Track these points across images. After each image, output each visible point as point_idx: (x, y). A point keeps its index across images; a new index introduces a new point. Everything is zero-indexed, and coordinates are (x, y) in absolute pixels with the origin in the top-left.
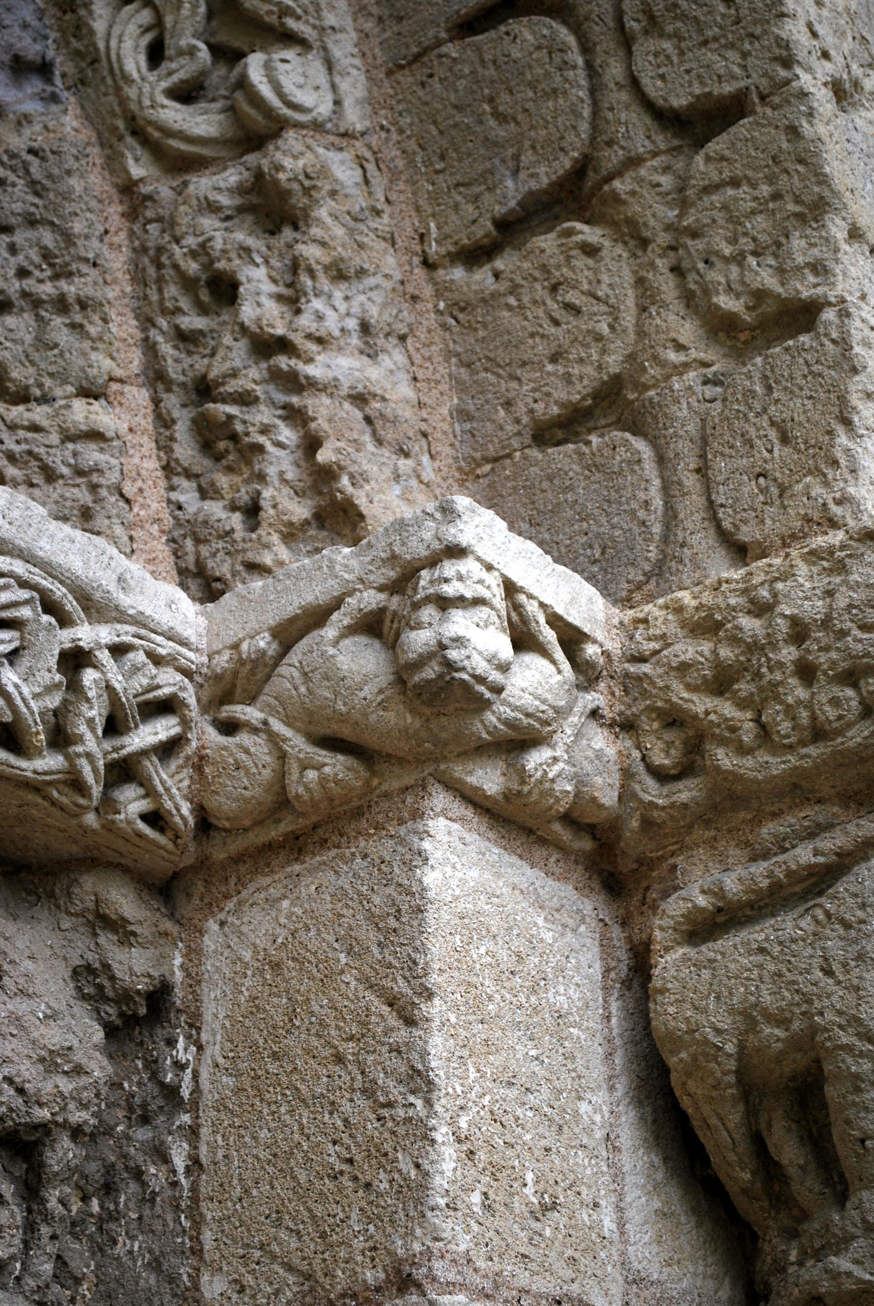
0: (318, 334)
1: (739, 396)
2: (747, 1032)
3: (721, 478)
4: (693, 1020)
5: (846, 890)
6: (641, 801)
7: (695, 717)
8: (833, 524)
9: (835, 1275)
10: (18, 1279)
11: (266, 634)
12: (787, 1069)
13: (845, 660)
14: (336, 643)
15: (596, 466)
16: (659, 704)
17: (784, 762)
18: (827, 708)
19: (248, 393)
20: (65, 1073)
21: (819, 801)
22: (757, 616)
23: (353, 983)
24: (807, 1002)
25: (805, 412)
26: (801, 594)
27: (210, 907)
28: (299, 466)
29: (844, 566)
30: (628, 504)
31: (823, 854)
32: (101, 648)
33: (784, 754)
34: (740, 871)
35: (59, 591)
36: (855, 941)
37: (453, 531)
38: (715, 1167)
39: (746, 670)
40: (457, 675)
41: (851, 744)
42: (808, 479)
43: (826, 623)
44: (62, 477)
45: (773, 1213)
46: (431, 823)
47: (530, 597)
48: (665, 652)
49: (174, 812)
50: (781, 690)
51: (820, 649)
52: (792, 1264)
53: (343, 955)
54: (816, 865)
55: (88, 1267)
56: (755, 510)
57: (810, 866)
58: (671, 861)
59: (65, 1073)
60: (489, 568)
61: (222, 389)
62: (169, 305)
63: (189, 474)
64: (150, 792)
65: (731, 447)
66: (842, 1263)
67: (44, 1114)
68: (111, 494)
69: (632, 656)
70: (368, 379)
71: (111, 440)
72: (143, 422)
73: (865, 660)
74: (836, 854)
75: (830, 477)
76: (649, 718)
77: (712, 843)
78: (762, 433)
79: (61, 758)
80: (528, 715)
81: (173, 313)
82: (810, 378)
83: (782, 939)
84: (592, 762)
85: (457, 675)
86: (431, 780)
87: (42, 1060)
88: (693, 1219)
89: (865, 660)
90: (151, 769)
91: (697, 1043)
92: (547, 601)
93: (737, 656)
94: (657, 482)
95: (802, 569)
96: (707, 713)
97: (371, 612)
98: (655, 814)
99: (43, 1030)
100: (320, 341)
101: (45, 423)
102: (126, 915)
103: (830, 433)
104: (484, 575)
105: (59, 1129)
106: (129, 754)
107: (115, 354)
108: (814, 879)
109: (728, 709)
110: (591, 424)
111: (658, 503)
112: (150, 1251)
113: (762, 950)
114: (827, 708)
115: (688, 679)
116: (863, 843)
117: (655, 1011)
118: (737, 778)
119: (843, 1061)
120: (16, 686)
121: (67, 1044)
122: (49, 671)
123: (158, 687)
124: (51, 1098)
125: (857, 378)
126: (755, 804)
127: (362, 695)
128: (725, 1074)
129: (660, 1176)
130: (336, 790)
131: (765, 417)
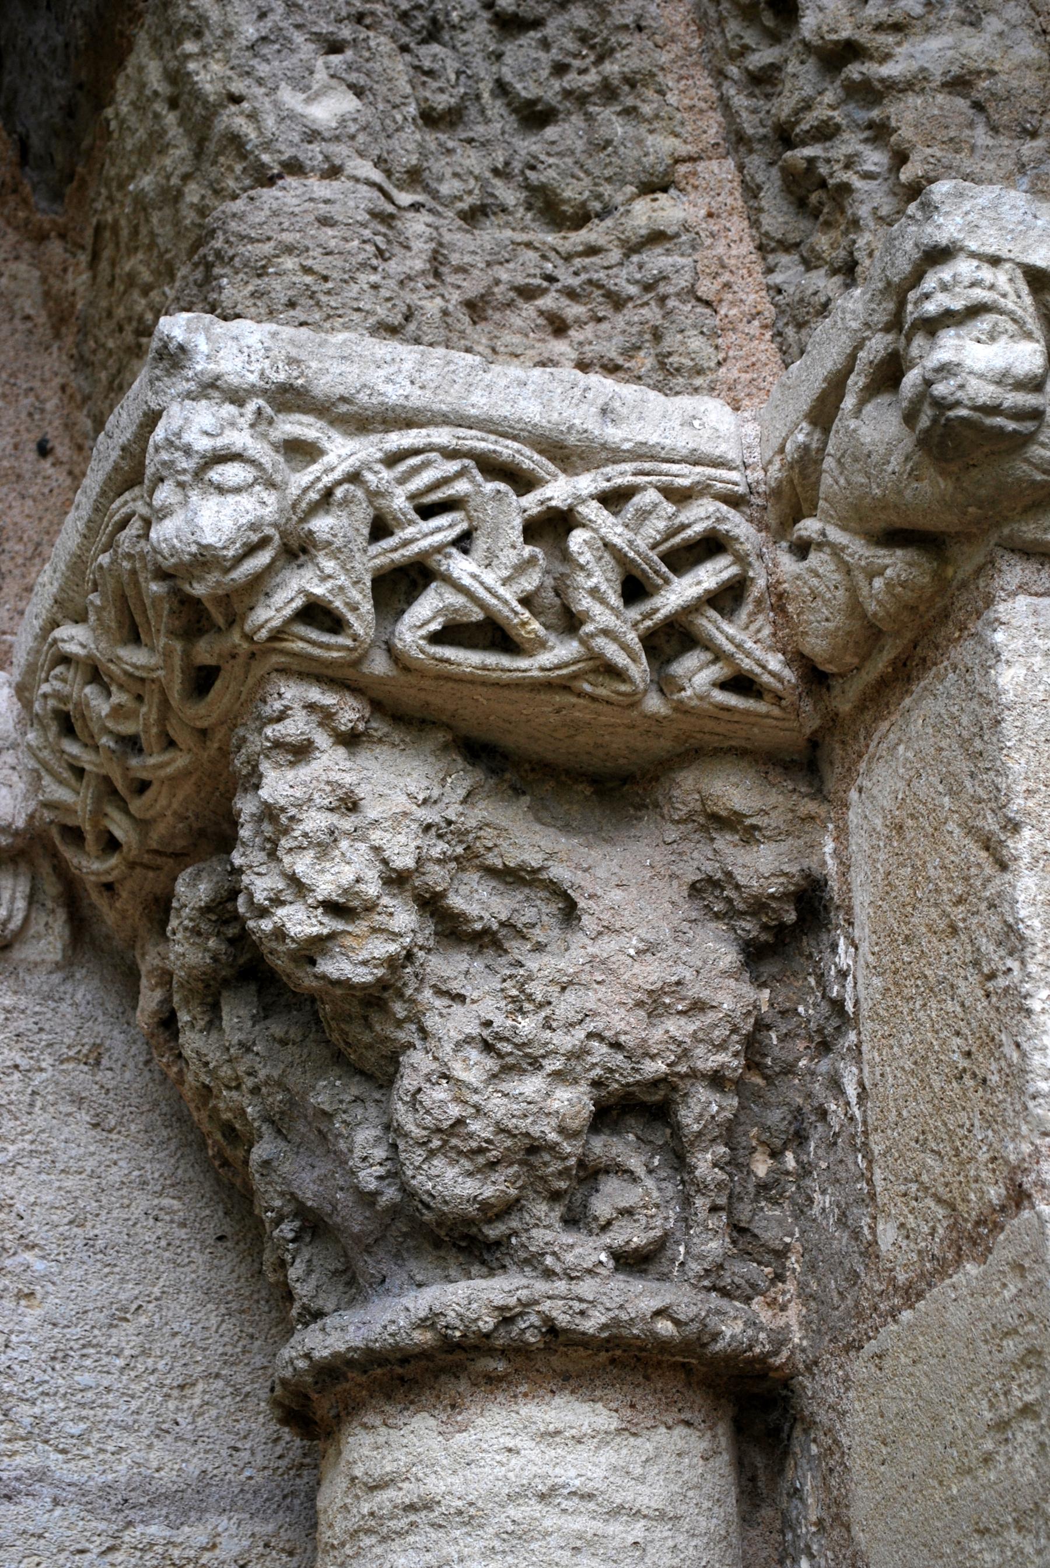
0: (891, 21)
10: (682, 1264)
11: (804, 424)
14: (857, 412)
19: (825, 123)
20: (679, 1013)
23: (957, 831)
27: (850, 774)
28: (895, 194)
32: (584, 501)
35: (507, 449)
40: (951, 414)
44: (630, 298)
46: (1001, 607)
49: (758, 670)
53: (946, 799)
55: (792, 1235)
59: (679, 1013)
60: (995, 261)
61: (797, 130)
62: (734, 46)
63: (786, 246)
64: (718, 656)
67: (660, 1067)
68: (684, 302)
70: (965, 56)
71: (677, 235)
72: (730, 201)
79: (575, 644)
81: (742, 55)
85: (951, 414)
86: (1000, 552)
87: (640, 1004)
90: (710, 627)
97: (883, 362)
99: (637, 968)
100: (897, 28)
101: (602, 241)
102: (737, 808)
104: (987, 274)
105: (688, 1082)
106: (667, 617)
107: (678, 129)
112: (838, 1206)
120: (474, 576)
121: (675, 979)
122: (514, 547)
123: (684, 527)
124: (662, 1047)
127: (890, 469)
130: (909, 596)
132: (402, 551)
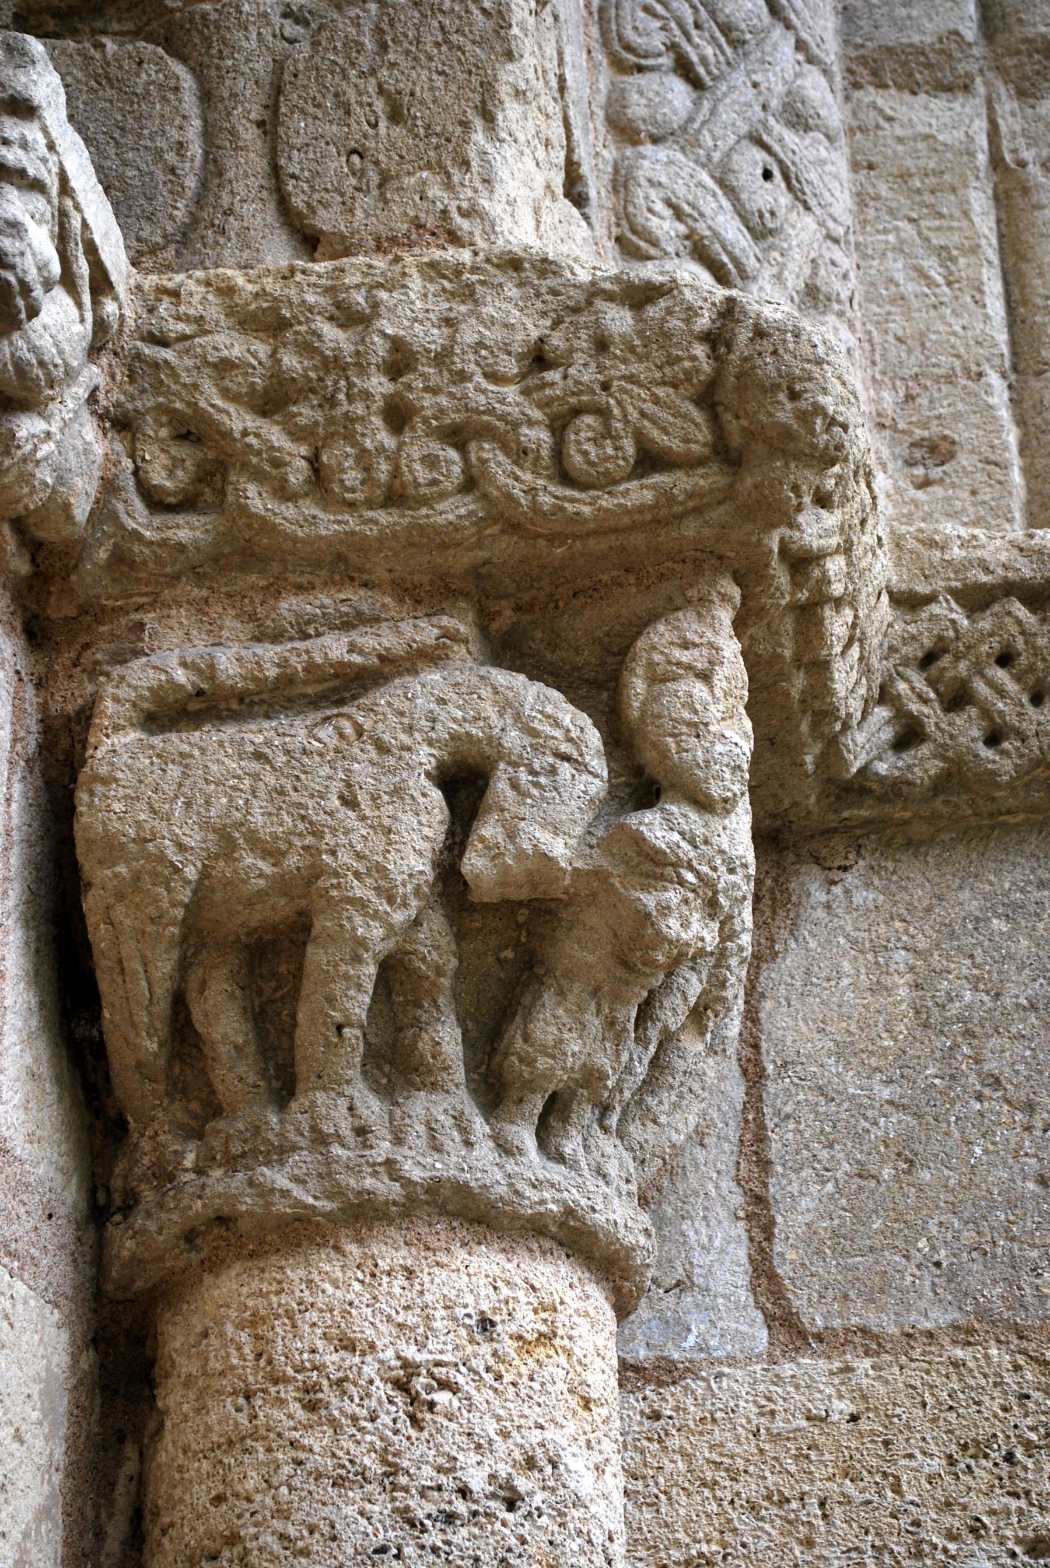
1: (339, 45)
2: (217, 857)
3: (297, 141)
4: (147, 826)
5: (389, 704)
6: (121, 527)
7: (228, 434)
8: (454, 238)
9: (266, 1192)
12: (257, 917)
13: (458, 411)
15: (109, 79)
16: (178, 405)
17: (339, 522)
18: (417, 466)
21: (365, 585)
22: (341, 326)
24: (313, 834)
25: (431, 89)
26: (409, 313)
29: (472, 293)
30: (152, 140)
31: (361, 652)
33: (342, 513)
34: (235, 649)
36: (393, 771)
37: (23, 79)
38: (106, 1026)
39: (312, 391)
41: (440, 520)
42: (425, 174)
43: (442, 358)
45: (166, 1102)
47: (77, 207)
48: (197, 340)
50: (359, 428)
51: (427, 389)
52: (187, 1170)
54: (350, 664)
56: (342, 195)
57: (341, 664)
58: (136, 616)
65: (318, 106)
66: (279, 1178)
69: (151, 334)
73: (486, 418)
74: (380, 657)
75: (456, 179)
76: (156, 421)
77: (201, 607)
78: (365, 98)
80: (42, 364)
82: (444, 48)
83: (290, 747)
84: (78, 455)
88: (56, 1089)
89: (486, 418)
91: (148, 857)
92: (90, 222)
93: (305, 370)
94: (197, 123)
95: (416, 283)
96: (245, 433)
98: (136, 548)
103: (465, 124)
108: (337, 683)
109: (276, 435)
110: (99, 25)
111: (196, 149)
113: (259, 756)
114: (417, 466)
115: (227, 383)
116: (418, 650)
117: (91, 805)
118: (267, 527)
119: (349, 919)
125: (510, 67)
126: (276, 568)
128: (174, 905)
129: (34, 1023)
131: (373, 81)
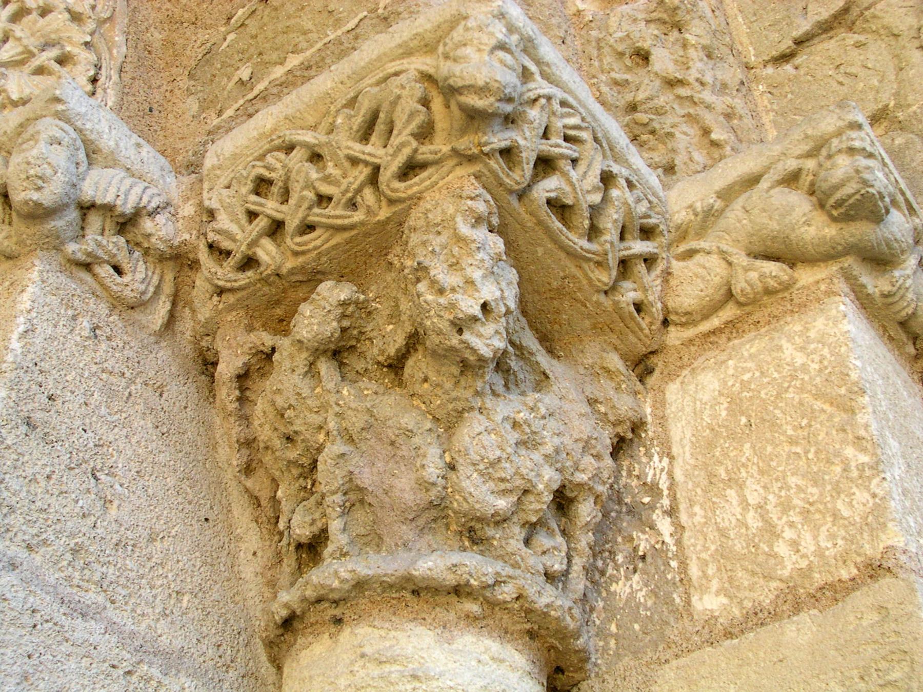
132: (553, 149)
